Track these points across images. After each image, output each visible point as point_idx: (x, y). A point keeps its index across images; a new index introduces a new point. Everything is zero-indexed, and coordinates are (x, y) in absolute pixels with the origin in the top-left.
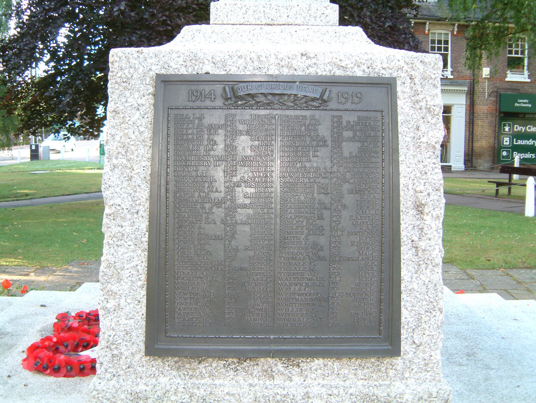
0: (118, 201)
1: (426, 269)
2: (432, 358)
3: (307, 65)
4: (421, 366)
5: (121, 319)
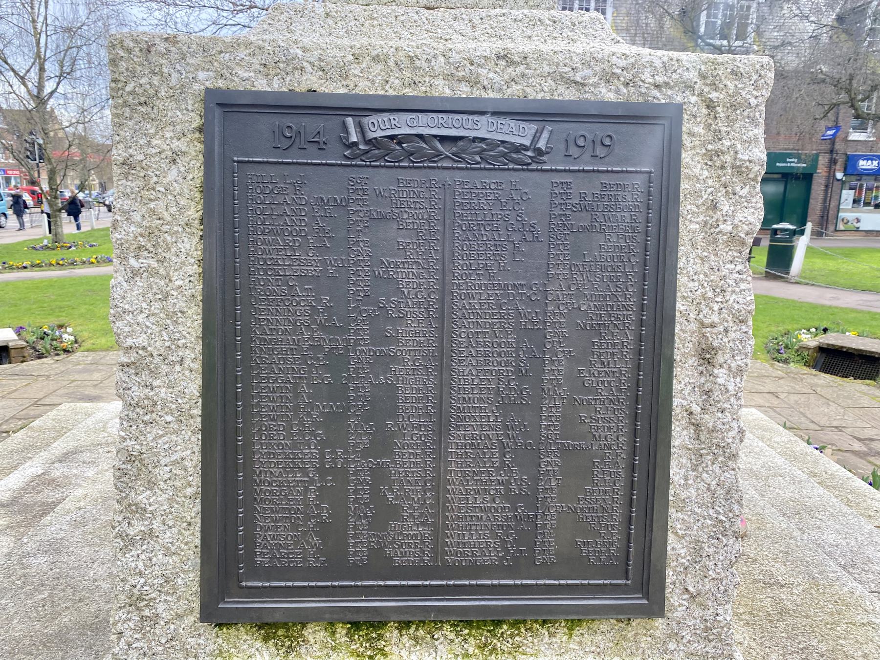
0: (142, 340)
1: (713, 463)
2: (718, 618)
3: (506, 77)
4: (698, 632)
5: (156, 556)
